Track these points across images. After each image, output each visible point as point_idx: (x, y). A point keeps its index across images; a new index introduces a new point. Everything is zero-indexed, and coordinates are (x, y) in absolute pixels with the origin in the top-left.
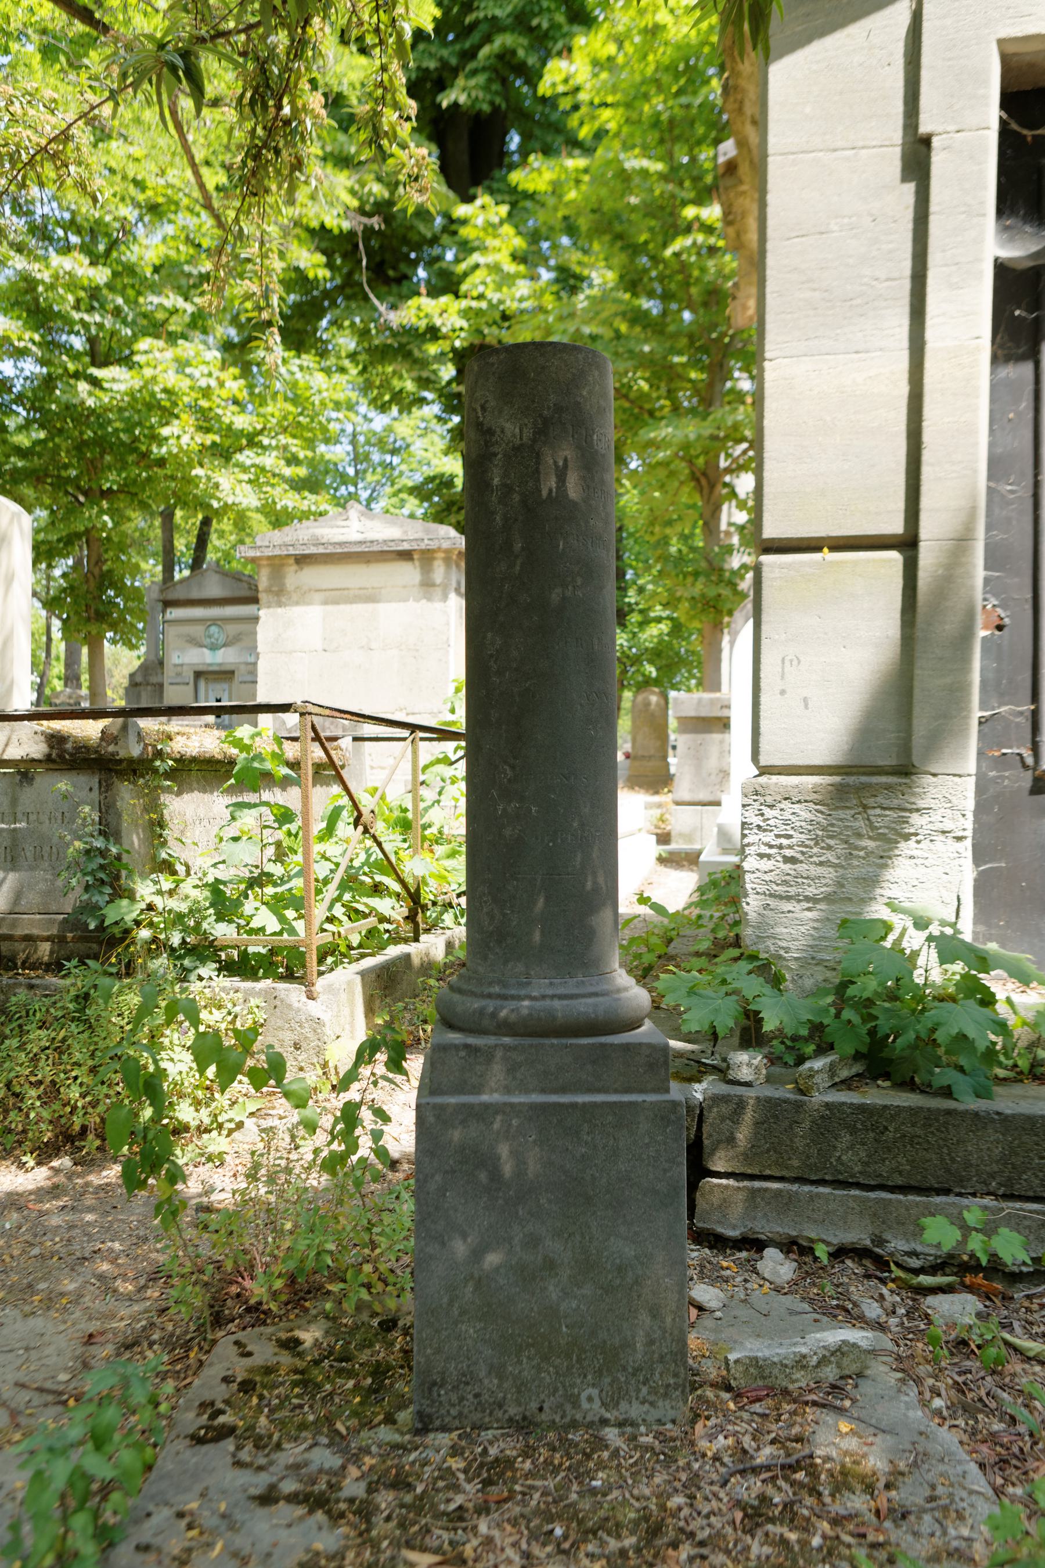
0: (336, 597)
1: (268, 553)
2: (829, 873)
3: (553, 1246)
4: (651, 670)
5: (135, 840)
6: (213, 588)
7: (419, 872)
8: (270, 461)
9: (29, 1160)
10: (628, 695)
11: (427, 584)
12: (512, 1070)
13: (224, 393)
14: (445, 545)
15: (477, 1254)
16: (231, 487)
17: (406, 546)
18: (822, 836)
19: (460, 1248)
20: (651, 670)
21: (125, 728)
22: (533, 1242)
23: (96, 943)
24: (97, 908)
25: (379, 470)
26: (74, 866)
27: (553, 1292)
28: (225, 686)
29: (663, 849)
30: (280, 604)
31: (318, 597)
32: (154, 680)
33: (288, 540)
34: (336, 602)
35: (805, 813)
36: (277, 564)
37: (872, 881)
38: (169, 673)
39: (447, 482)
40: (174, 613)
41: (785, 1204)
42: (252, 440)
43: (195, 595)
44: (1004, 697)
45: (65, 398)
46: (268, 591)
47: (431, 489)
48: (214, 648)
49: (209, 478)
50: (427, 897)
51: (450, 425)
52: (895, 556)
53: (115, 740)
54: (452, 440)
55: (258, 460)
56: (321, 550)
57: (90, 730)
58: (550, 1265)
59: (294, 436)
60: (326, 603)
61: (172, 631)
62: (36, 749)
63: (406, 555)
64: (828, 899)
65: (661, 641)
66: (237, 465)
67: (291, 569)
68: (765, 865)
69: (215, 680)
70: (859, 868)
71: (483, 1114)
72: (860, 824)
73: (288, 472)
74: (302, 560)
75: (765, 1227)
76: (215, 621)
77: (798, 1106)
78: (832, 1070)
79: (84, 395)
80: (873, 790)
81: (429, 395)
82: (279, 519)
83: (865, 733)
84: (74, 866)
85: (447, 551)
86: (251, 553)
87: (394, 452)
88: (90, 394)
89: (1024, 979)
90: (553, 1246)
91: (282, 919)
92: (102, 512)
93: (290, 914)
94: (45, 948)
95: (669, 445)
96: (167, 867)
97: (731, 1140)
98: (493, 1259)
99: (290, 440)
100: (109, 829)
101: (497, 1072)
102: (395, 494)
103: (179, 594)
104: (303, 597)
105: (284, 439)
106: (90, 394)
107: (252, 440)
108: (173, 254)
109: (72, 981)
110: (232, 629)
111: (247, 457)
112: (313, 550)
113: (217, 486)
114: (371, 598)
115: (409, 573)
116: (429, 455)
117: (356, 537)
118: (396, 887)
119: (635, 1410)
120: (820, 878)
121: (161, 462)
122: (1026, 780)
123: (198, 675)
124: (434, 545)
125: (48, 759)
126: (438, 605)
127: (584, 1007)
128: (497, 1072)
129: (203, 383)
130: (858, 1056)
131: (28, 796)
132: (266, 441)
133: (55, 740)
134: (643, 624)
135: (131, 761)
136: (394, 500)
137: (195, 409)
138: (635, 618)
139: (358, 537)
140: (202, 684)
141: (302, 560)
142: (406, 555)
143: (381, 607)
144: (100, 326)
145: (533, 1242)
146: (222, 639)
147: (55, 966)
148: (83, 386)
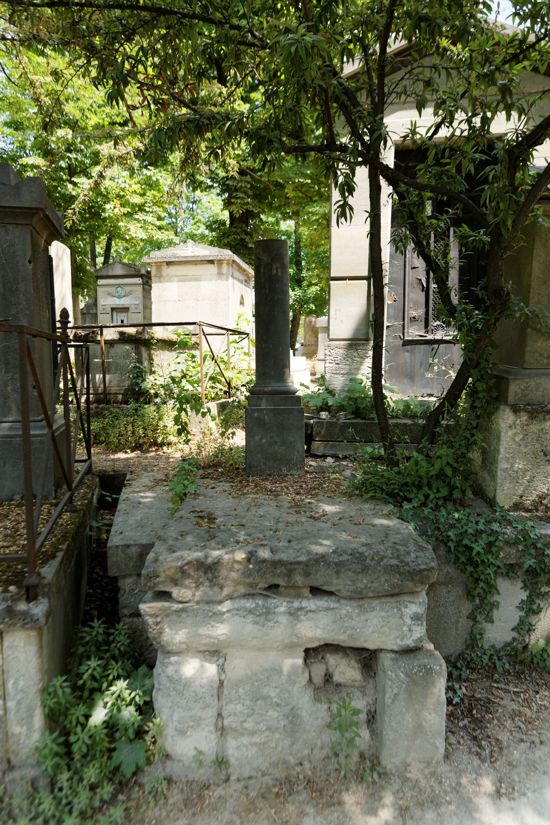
0: (183, 279)
1: (155, 260)
2: (347, 367)
3: (276, 438)
4: (312, 306)
5: (146, 363)
6: (118, 270)
7: (231, 376)
8: (150, 218)
9: (129, 451)
10: (303, 318)
11: (220, 274)
12: (267, 401)
13: (131, 190)
14: (227, 258)
15: (260, 440)
16: (135, 230)
17: (211, 258)
18: (346, 357)
19: (257, 438)
20: (312, 306)
21: (144, 330)
22: (272, 437)
23: (138, 395)
24: (138, 384)
25: (187, 212)
26: (130, 372)
27: (276, 448)
28: (125, 314)
29: (313, 378)
30: (160, 282)
31: (176, 278)
32: (92, 312)
33: (163, 255)
34: (183, 281)
35: (341, 351)
36: (159, 265)
37: (358, 369)
38: (100, 309)
39: (223, 223)
40: (101, 282)
41: (333, 447)
42: (141, 208)
43: (110, 273)
44: (396, 320)
45: (63, 191)
46: (156, 276)
47: (214, 225)
48: (119, 297)
49: (126, 226)
50: (233, 385)
51: (224, 197)
52: (365, 282)
53: (141, 333)
54: (224, 204)
55: (145, 218)
56: (177, 260)
57: (132, 331)
58: (276, 442)
59: (159, 207)
60: (179, 281)
61: (100, 290)
62: (116, 337)
63: (211, 262)
64: (347, 374)
65: (317, 294)
66: (135, 219)
67: (165, 267)
68: (331, 365)
69: (121, 312)
70: (355, 365)
71: (261, 410)
72: (355, 354)
73: (158, 223)
74: (169, 263)
75: (328, 452)
76: (119, 285)
77: (336, 423)
78: (345, 415)
79: (71, 190)
80: (359, 345)
81: (215, 185)
82: (158, 246)
83: (357, 330)
84: (130, 372)
85: (228, 260)
86: (148, 261)
87: (194, 202)
88: (73, 190)
89: (392, 391)
90: (276, 438)
91: (194, 387)
92: (78, 240)
93: (196, 385)
94: (120, 397)
95: (317, 214)
96: (154, 372)
97: (320, 433)
98: (264, 441)
99: (158, 209)
100: (140, 361)
101: (264, 401)
102: (195, 224)
103: (100, 274)
104: (170, 279)
105: (156, 209)
106: (73, 190)
107: (141, 208)
108: (101, 121)
109: (132, 405)
110: (128, 289)
111: (140, 216)
112: (174, 260)
113: (129, 230)
114: (197, 279)
115: (213, 269)
116: (211, 205)
117: (191, 254)
118: (223, 380)
119: (294, 472)
120: (345, 369)
121: (105, 219)
122: (401, 342)
123: (113, 309)
124: (222, 258)
125: (120, 339)
126: (225, 282)
127: (283, 388)
128: (264, 401)
129: (123, 186)
130: (353, 413)
131: (112, 351)
132: (147, 209)
133: (122, 334)
134: (310, 285)
135: (145, 340)
136: (195, 226)
137: (118, 196)
138: (305, 283)
139: (192, 254)
140: (115, 313)
141: (169, 263)
142: (211, 262)
143: (202, 283)
144: (76, 159)
145: (272, 437)
146: (123, 295)
147: (126, 402)
148: (70, 186)
